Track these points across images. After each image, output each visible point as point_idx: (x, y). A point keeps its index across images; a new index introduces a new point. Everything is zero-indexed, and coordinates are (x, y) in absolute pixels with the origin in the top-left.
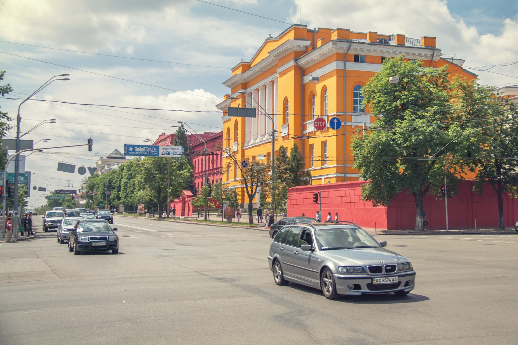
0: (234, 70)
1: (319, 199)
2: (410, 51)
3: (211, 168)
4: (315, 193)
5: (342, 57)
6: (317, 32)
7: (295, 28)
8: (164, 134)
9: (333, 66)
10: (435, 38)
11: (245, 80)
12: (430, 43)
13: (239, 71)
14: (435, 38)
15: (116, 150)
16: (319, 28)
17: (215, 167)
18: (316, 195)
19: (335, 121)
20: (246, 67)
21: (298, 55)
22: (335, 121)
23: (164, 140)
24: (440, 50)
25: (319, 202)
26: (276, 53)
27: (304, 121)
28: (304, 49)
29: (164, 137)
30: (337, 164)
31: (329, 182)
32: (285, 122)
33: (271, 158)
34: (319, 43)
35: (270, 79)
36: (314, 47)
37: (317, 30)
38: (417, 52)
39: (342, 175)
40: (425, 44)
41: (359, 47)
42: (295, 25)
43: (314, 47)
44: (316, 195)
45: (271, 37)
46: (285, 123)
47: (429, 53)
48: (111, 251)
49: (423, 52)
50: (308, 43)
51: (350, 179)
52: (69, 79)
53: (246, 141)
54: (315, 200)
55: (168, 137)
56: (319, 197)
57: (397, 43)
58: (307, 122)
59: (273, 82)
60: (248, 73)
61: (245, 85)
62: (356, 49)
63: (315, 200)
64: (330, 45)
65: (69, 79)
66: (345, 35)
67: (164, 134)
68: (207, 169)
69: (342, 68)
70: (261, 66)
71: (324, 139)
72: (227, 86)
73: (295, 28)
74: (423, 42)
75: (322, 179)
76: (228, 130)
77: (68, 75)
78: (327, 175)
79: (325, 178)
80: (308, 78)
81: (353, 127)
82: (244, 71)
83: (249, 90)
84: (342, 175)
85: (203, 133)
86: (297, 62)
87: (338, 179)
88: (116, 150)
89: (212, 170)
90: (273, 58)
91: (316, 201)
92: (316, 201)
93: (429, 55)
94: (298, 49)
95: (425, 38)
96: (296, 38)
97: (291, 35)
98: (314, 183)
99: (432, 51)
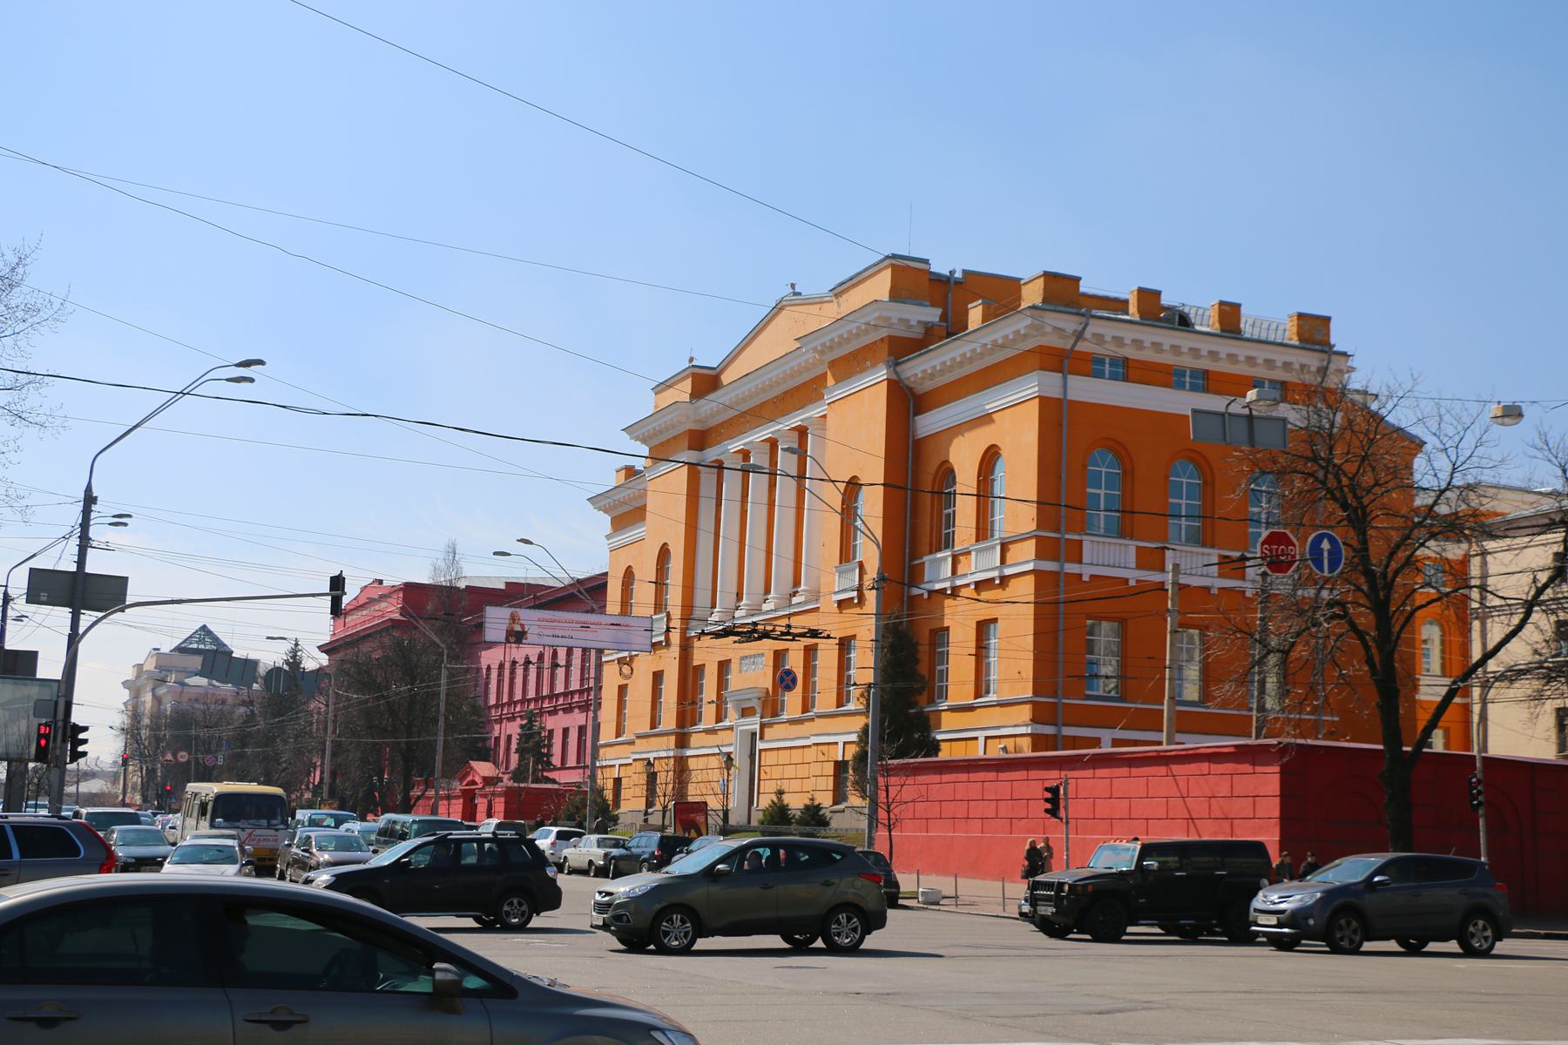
0: (660, 388)
1: (1062, 803)
2: (1261, 354)
3: (531, 694)
4: (1048, 784)
6: (958, 283)
8: (381, 582)
9: (1028, 388)
10: (1328, 319)
11: (700, 421)
12: (1313, 330)
13: (684, 390)
14: (1328, 319)
15: (204, 628)
16: (965, 272)
17: (560, 688)
18: (1054, 791)
19: (1326, 545)
20: (705, 382)
21: (901, 348)
22: (1326, 545)
23: (382, 598)
24: (1344, 354)
25: (1062, 813)
27: (915, 554)
28: (918, 333)
30: (1035, 693)
31: (1005, 749)
32: (846, 552)
35: (795, 420)
36: (953, 326)
37: (958, 275)
38: (1280, 357)
40: (1299, 334)
41: (1109, 331)
42: (894, 256)
44: (1054, 791)
46: (848, 560)
47: (1313, 360)
48: (652, 947)
50: (932, 315)
51: (1074, 742)
52: (251, 380)
53: (697, 613)
54: (1049, 806)
55: (394, 590)
57: (1217, 325)
58: (926, 558)
59: (802, 432)
60: (711, 406)
61: (700, 439)
62: (1099, 338)
63: (1049, 806)
64: (1015, 325)
65: (251, 380)
67: (381, 582)
68: (518, 696)
69: (1055, 392)
71: (985, 612)
72: (637, 439)
74: (1295, 329)
76: (629, 576)
77: (261, 362)
78: (998, 728)
79: (987, 738)
80: (929, 423)
82: (697, 394)
83: (712, 454)
84: (1049, 730)
86: (899, 369)
87: (1038, 741)
88: (204, 628)
91: (1054, 812)
92: (1054, 812)
93: (1313, 369)
95: (1301, 316)
96: (896, 295)
97: (881, 286)
98: (945, 754)
99: (1325, 356)
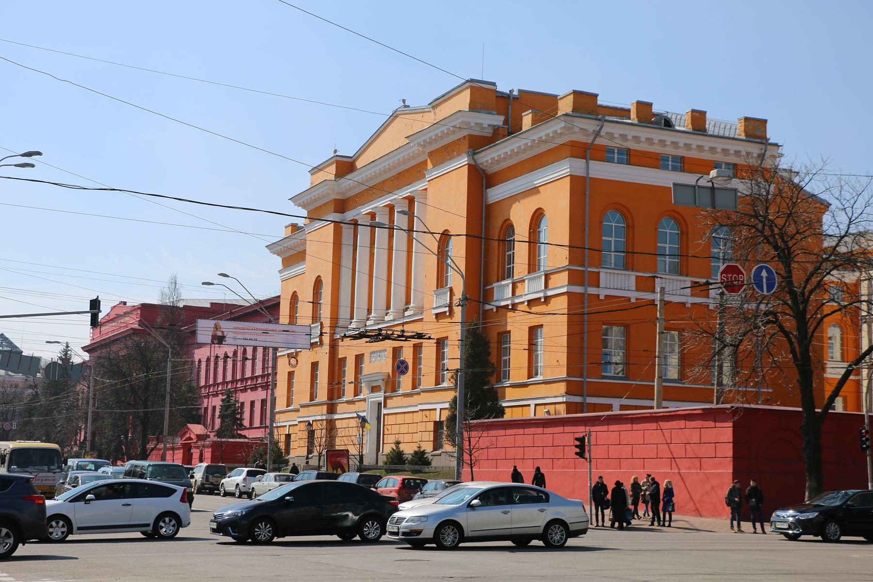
0: (315, 170)
1: (587, 448)
2: (720, 145)
3: (229, 378)
4: (577, 436)
5: (583, 151)
7: (471, 87)
10: (765, 121)
12: (755, 129)
14: (765, 121)
17: (248, 374)
18: (582, 440)
20: (345, 166)
23: (126, 314)
24: (776, 145)
25: (587, 455)
26: (427, 137)
27: (487, 282)
28: (488, 132)
29: (121, 312)
30: (568, 375)
31: (548, 412)
33: (270, 364)
34: (527, 120)
35: (406, 192)
37: (515, 93)
38: (732, 147)
39: (578, 399)
40: (745, 131)
41: (617, 130)
43: (512, 128)
44: (582, 440)
45: (406, 106)
47: (755, 149)
49: (745, 148)
52: (33, 166)
54: (578, 450)
55: (134, 308)
56: (586, 443)
58: (494, 285)
59: (411, 200)
60: (349, 183)
62: (610, 135)
63: (578, 450)
65: (33, 166)
66: (585, 103)
67: (125, 303)
68: (220, 379)
69: (581, 173)
70: (377, 169)
71: (534, 320)
72: (299, 205)
73: (471, 87)
74: (743, 128)
75: (529, 405)
76: (294, 298)
77: (39, 153)
79: (536, 405)
80: (496, 194)
81: (602, 297)
82: (339, 175)
83: (350, 215)
85: (208, 306)
86: (476, 157)
87: (571, 407)
89: (232, 382)
90: (416, 148)
91: (581, 454)
92: (581, 454)
93: (755, 155)
94: (477, 132)
95: (747, 119)
96: (474, 107)
97: (463, 101)
98: (508, 416)
